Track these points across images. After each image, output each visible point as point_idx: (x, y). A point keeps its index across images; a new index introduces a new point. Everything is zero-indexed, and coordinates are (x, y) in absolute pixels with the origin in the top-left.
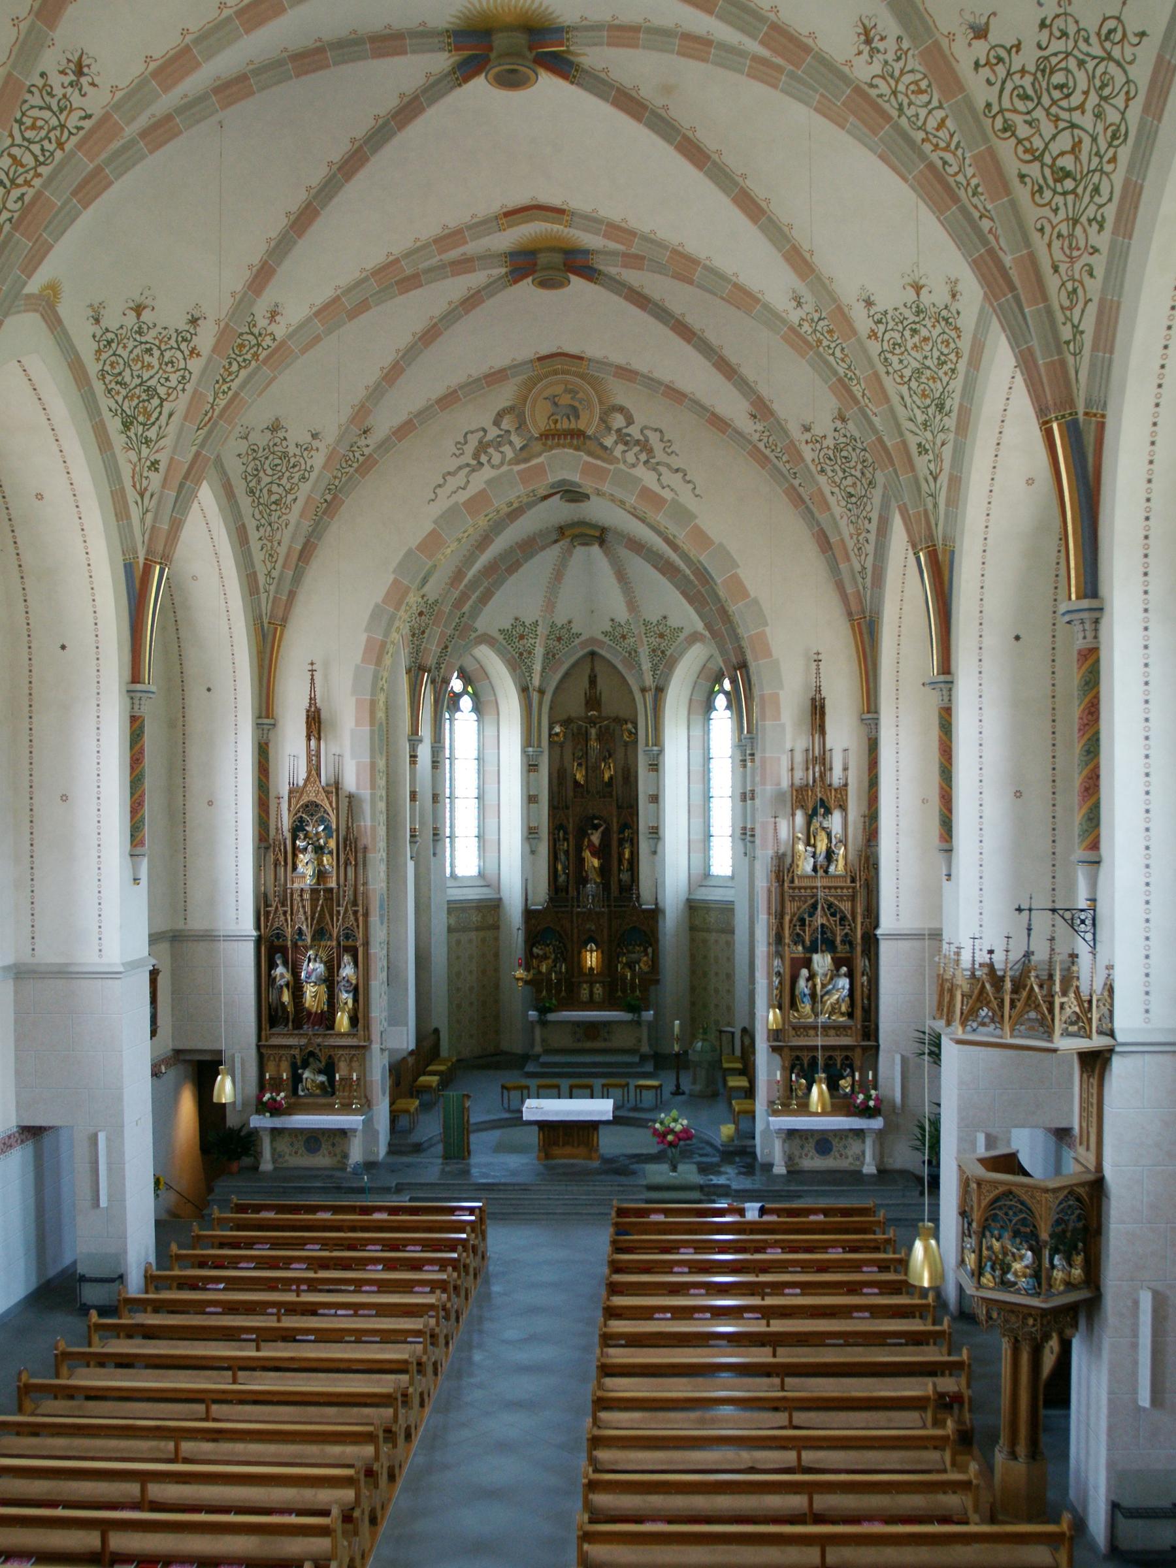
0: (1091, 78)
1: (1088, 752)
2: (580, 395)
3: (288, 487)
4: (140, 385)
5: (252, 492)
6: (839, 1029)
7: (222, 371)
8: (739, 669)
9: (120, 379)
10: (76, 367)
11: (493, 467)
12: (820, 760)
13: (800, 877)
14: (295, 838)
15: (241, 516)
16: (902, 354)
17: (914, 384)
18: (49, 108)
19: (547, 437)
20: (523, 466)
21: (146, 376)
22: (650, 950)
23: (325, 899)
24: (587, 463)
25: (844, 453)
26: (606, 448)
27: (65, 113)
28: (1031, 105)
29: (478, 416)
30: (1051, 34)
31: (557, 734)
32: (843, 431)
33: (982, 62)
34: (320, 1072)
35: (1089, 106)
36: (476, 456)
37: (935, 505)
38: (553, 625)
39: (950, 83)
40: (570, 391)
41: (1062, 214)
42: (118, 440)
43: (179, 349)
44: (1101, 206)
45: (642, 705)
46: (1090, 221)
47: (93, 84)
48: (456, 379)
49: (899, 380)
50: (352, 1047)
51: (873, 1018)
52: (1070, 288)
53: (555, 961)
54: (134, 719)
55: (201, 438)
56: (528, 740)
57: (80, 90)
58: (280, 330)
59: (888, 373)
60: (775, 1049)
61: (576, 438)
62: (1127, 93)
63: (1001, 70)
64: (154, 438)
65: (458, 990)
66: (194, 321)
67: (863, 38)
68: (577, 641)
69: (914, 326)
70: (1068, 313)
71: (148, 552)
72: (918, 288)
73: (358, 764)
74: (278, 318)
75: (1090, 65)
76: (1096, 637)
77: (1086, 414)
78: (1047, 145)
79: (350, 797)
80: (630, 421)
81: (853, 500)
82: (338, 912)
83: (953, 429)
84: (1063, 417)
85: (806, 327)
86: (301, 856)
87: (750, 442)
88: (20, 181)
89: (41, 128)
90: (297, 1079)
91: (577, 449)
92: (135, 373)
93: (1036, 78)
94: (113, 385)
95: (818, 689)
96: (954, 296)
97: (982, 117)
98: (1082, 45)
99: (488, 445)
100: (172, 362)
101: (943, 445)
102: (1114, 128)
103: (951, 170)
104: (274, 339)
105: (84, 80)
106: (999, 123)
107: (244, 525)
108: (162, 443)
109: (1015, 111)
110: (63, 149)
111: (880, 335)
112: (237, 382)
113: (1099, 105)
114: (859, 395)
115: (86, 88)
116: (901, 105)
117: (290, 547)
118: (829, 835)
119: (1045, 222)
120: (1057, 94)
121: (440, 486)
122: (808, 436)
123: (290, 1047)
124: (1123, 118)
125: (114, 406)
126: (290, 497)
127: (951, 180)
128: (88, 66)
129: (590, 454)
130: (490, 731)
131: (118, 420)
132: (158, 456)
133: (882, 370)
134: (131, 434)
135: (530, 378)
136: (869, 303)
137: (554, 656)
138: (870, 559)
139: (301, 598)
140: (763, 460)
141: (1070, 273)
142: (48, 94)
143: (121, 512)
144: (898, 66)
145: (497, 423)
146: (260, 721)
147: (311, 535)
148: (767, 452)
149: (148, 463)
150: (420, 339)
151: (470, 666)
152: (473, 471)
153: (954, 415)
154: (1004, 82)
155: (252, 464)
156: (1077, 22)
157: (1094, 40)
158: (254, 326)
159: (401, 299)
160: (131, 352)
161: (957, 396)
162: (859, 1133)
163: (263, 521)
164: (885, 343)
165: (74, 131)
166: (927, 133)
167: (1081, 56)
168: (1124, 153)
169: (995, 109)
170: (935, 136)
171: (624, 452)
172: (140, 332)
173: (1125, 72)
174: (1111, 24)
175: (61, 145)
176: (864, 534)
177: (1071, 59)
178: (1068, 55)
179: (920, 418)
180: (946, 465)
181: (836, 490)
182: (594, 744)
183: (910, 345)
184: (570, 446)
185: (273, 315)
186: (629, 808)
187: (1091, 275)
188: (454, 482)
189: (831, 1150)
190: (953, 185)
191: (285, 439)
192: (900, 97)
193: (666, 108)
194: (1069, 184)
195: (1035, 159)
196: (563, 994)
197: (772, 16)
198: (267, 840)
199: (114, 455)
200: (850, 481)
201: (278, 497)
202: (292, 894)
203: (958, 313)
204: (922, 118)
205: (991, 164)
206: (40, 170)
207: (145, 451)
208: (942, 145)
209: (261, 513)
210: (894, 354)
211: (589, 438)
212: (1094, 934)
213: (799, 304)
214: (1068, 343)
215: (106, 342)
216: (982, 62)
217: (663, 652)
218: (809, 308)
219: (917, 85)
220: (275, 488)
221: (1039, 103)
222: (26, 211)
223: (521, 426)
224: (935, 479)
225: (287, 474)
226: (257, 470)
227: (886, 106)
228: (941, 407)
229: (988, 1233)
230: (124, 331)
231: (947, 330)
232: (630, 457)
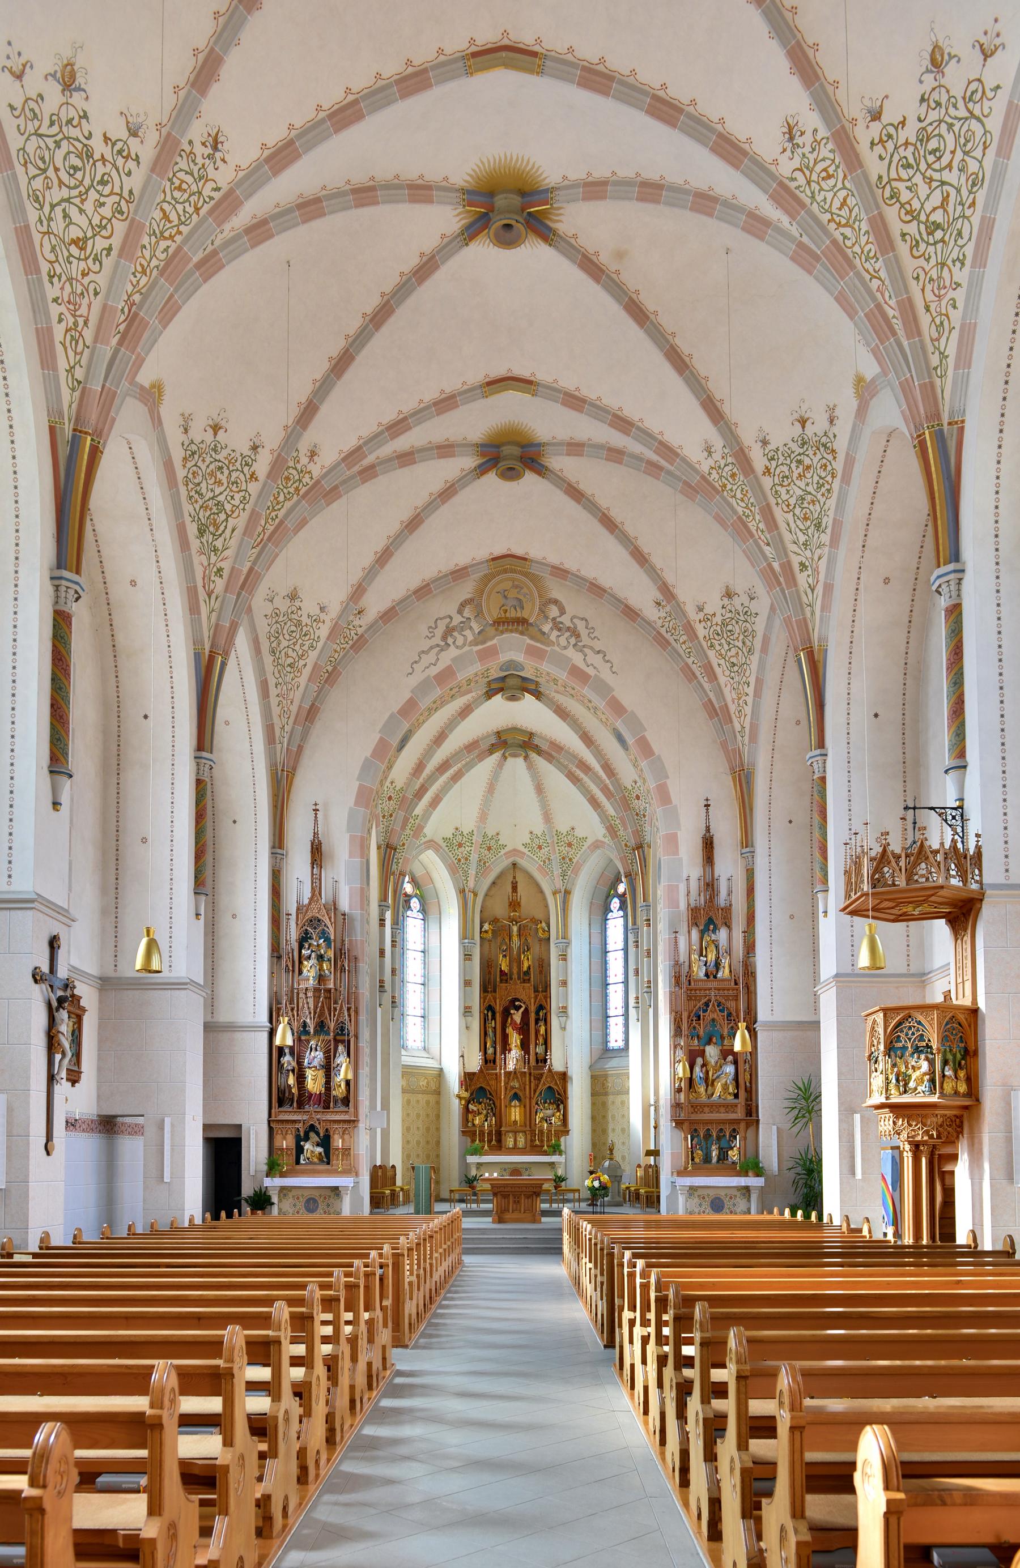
0: (956, 140)
1: (955, 683)
2: (525, 590)
3: (300, 653)
4: (212, 498)
5: (273, 652)
6: (730, 1107)
7: (272, 498)
8: (637, 848)
9: (198, 488)
10: (168, 465)
11: (457, 647)
12: (710, 886)
13: (695, 981)
14: (301, 947)
15: (264, 672)
16: (789, 484)
17: (797, 511)
18: (192, 175)
19: (499, 623)
20: (480, 647)
21: (217, 491)
22: (561, 1106)
23: (325, 998)
24: (528, 644)
25: (730, 628)
26: (544, 633)
27: (203, 181)
28: (911, 172)
29: (445, 606)
30: (929, 106)
31: (486, 932)
32: (729, 607)
33: (876, 141)
34: (318, 1145)
35: (955, 164)
36: (444, 638)
37: (813, 613)
38: (485, 835)
39: (852, 160)
40: (517, 587)
41: (933, 261)
42: (195, 544)
43: (242, 472)
44: (962, 247)
45: (554, 905)
46: (954, 261)
47: (223, 160)
48: (429, 573)
49: (785, 509)
50: (344, 1121)
51: (754, 1098)
52: (938, 323)
53: (486, 1116)
54: (199, 782)
55: (254, 556)
56: (465, 935)
57: (215, 163)
58: (316, 471)
59: (777, 504)
60: (679, 1124)
61: (521, 624)
62: (985, 143)
63: (890, 146)
64: (220, 548)
65: (408, 1142)
66: (255, 448)
67: (787, 136)
68: (503, 852)
69: (799, 458)
70: (936, 343)
71: (212, 646)
72: (803, 422)
73: (351, 889)
74: (315, 458)
75: (956, 129)
76: (959, 596)
77: (950, 424)
78: (922, 205)
79: (344, 915)
80: (562, 611)
81: (736, 668)
82: (335, 1009)
83: (827, 543)
84: (933, 426)
85: (715, 475)
86: (305, 963)
87: (654, 629)
88: (167, 234)
89: (185, 191)
90: (300, 1150)
91: (522, 633)
92: (210, 487)
93: (916, 148)
94: (193, 493)
95: (708, 829)
96: (831, 422)
97: (875, 188)
98: (952, 111)
99: (453, 629)
100: (237, 483)
101: (819, 559)
102: (974, 176)
103: (849, 243)
104: (312, 478)
105: (218, 155)
106: (887, 193)
107: (266, 679)
108: (226, 553)
109: (900, 180)
110: (198, 214)
111: (772, 471)
112: (283, 512)
113: (963, 160)
114: (753, 529)
115: (219, 163)
116: (813, 193)
117: (300, 707)
118: (717, 947)
119: (920, 270)
120: (931, 159)
121: (416, 662)
122: (701, 615)
123: (295, 1122)
124: (981, 166)
125: (193, 513)
126: (302, 663)
127: (849, 251)
128: (222, 143)
129: (532, 638)
130: (433, 928)
131: (195, 526)
132: (222, 564)
133: (772, 501)
134: (204, 540)
135: (485, 576)
136: (765, 443)
137: (485, 863)
138: (748, 718)
139: (307, 752)
140: (662, 642)
141: (938, 310)
142: (193, 161)
143: (193, 609)
144: (812, 157)
145: (460, 612)
146: (275, 851)
147: (315, 699)
148: (668, 636)
149: (215, 569)
150: (406, 527)
151: (419, 872)
152: (442, 650)
153: (829, 531)
154: (892, 156)
155: (275, 627)
156: (948, 92)
157: (961, 104)
158: (298, 461)
159: (399, 472)
160: (208, 466)
161: (831, 513)
162: (747, 1190)
163: (280, 680)
164: (776, 477)
165: (207, 200)
166: (832, 214)
167: (950, 121)
168: (981, 196)
169: (885, 180)
170: (839, 215)
171: (559, 636)
172: (215, 450)
173: (983, 126)
174: (974, 86)
175: (197, 210)
176: (744, 698)
177: (943, 124)
178: (940, 121)
179: (802, 538)
180: (822, 577)
181: (722, 662)
182: (515, 939)
183: (795, 475)
184: (516, 631)
185: (313, 454)
186: (544, 988)
187: (955, 307)
188: (427, 659)
189: (723, 1207)
190: (851, 255)
191: (300, 608)
192: (813, 185)
193: (618, 272)
194: (939, 234)
195: (914, 218)
196: (494, 1142)
197: (719, 127)
198: (278, 951)
199: (190, 555)
200: (733, 651)
201: (292, 661)
202: (298, 994)
203: (835, 436)
204: (828, 201)
205: (879, 228)
206: (182, 228)
207: (213, 559)
208: (843, 221)
209: (53, 249)
210: (782, 486)
211: (531, 624)
212: (963, 827)
213: (710, 453)
214: (935, 369)
215: (191, 454)
216: (876, 141)
217: (570, 860)
218: (717, 456)
219: (827, 172)
220: (290, 652)
221: (918, 169)
222: (169, 262)
223: (479, 614)
224: (813, 591)
225: (300, 641)
226: (42, 159)
227: (802, 196)
228: (818, 526)
229: (892, 1053)
230: (203, 446)
231: (825, 455)
232: (563, 641)
